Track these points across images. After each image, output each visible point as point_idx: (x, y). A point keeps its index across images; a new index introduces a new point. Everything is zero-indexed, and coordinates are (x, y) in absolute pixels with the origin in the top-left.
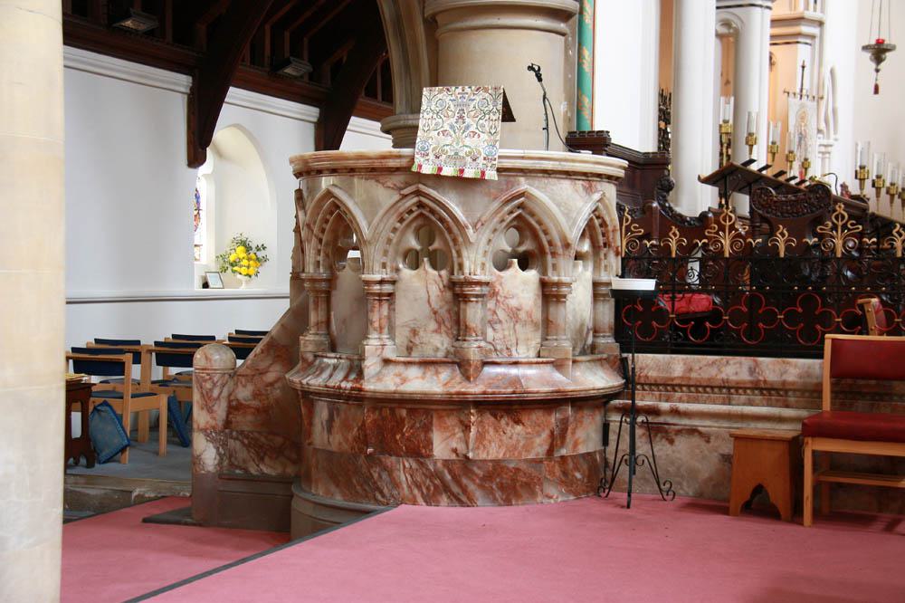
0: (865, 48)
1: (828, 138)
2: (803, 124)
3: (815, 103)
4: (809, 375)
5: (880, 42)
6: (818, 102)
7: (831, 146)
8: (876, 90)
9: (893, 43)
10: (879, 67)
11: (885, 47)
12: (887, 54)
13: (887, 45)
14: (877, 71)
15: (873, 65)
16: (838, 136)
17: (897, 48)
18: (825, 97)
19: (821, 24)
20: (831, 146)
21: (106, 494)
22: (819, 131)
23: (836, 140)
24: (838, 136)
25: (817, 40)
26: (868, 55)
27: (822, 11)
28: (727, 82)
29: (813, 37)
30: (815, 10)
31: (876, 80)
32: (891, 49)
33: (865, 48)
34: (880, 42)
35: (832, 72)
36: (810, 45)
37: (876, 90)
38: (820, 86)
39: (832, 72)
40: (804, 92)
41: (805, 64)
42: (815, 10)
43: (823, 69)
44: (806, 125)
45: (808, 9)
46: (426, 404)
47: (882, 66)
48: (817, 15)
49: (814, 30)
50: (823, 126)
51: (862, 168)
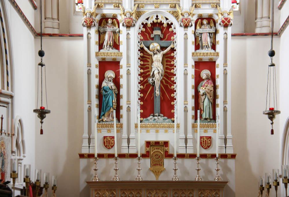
0: (35, 111)
1: (20, 155)
2: (3, 148)
3: (10, 137)
4: (122, 109)
5: (42, 108)
6: (12, 137)
7: (22, 160)
8: (42, 132)
9: (49, 109)
10: (43, 121)
11: (45, 111)
12: (47, 115)
13: (46, 110)
14: (42, 123)
15: (39, 120)
16: (25, 155)
17: (51, 112)
18: (16, 134)
19: (12, 97)
20: (22, 160)
21: (102, 94)
22: (13, 152)
23: (24, 157)
24: (25, 155)
25: (10, 105)
26: (36, 114)
27: (12, 91)
28: (281, 31)
29: (7, 103)
30: (8, 89)
31: (41, 127)
32: (48, 112)
33: (35, 111)
34: (42, 108)
35: (20, 121)
36: (6, 107)
37: (42, 132)
38: (13, 128)
39: (20, 121)
40: (3, 131)
41: (3, 117)
42: (8, 89)
43: (14, 120)
44: (4, 149)
45: (4, 89)
46: (19, 152)
47: (44, 120)
48: (9, 92)
49: (9, 100)
50: (15, 149)
51: (27, 177)
